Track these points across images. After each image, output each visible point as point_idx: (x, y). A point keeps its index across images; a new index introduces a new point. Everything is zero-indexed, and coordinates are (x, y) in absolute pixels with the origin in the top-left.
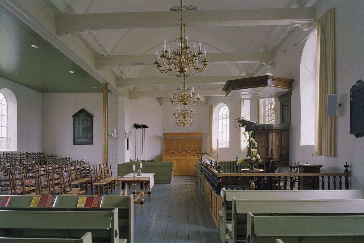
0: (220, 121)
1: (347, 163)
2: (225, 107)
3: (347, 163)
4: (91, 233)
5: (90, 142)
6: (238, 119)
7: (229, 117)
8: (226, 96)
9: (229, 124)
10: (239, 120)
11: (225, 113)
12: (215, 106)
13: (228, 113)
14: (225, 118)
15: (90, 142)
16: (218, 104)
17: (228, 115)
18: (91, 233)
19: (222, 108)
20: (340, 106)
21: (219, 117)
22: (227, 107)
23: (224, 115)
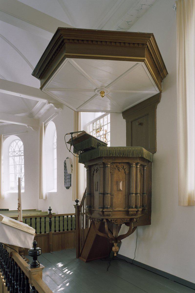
0: (11, 159)
1: (50, 207)
2: (17, 141)
3: (50, 207)
4: (56, 191)
5: (3, 217)
6: (72, 134)
7: (23, 154)
8: (41, 88)
9: (23, 163)
10: (73, 135)
11: (17, 149)
12: (5, 138)
13: (22, 149)
14: (17, 155)
15: (3, 217)
16: (7, 137)
17: (23, 152)
18: (56, 191)
19: (15, 143)
20: (68, 188)
21: (10, 154)
22: (21, 143)
23: (17, 152)
